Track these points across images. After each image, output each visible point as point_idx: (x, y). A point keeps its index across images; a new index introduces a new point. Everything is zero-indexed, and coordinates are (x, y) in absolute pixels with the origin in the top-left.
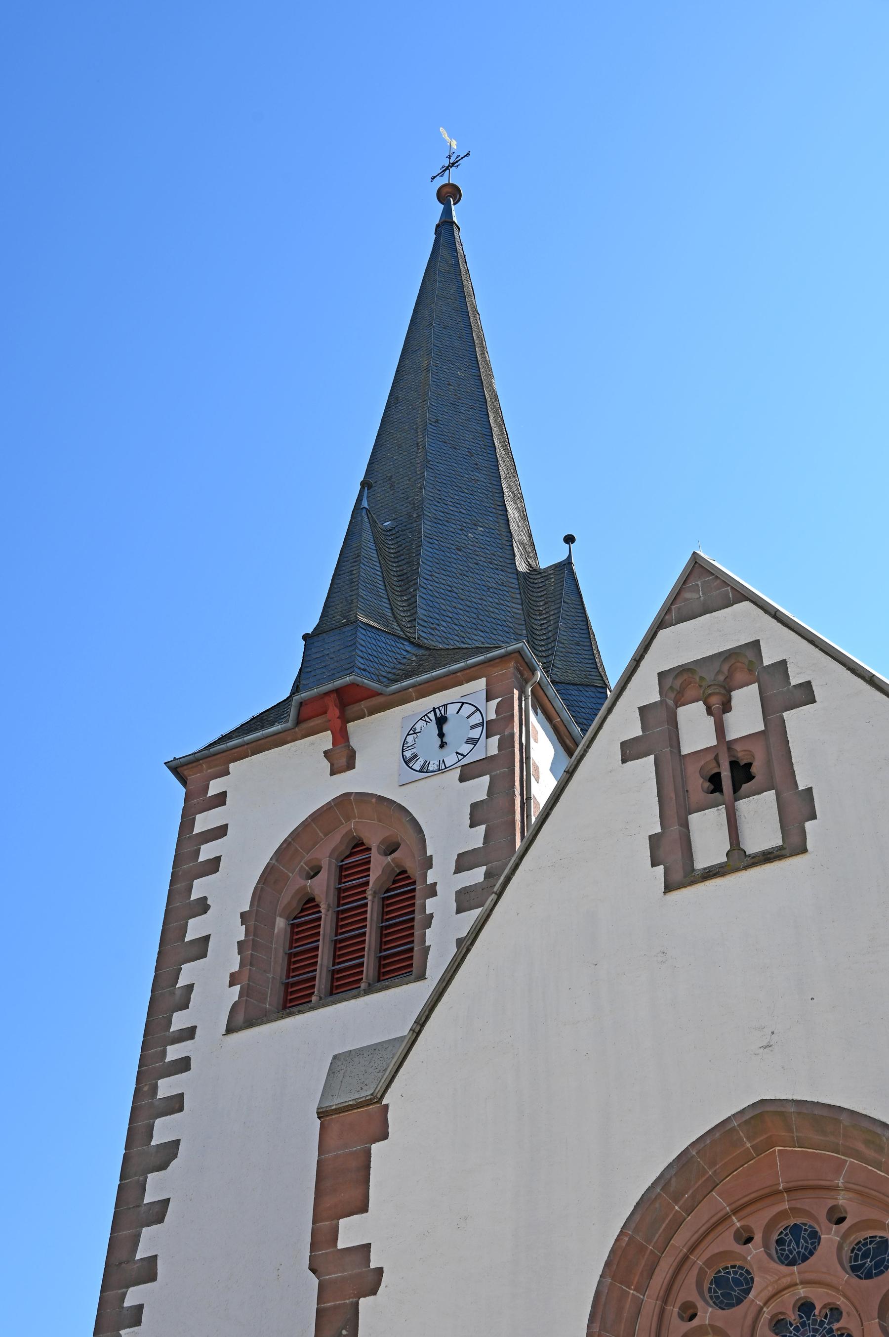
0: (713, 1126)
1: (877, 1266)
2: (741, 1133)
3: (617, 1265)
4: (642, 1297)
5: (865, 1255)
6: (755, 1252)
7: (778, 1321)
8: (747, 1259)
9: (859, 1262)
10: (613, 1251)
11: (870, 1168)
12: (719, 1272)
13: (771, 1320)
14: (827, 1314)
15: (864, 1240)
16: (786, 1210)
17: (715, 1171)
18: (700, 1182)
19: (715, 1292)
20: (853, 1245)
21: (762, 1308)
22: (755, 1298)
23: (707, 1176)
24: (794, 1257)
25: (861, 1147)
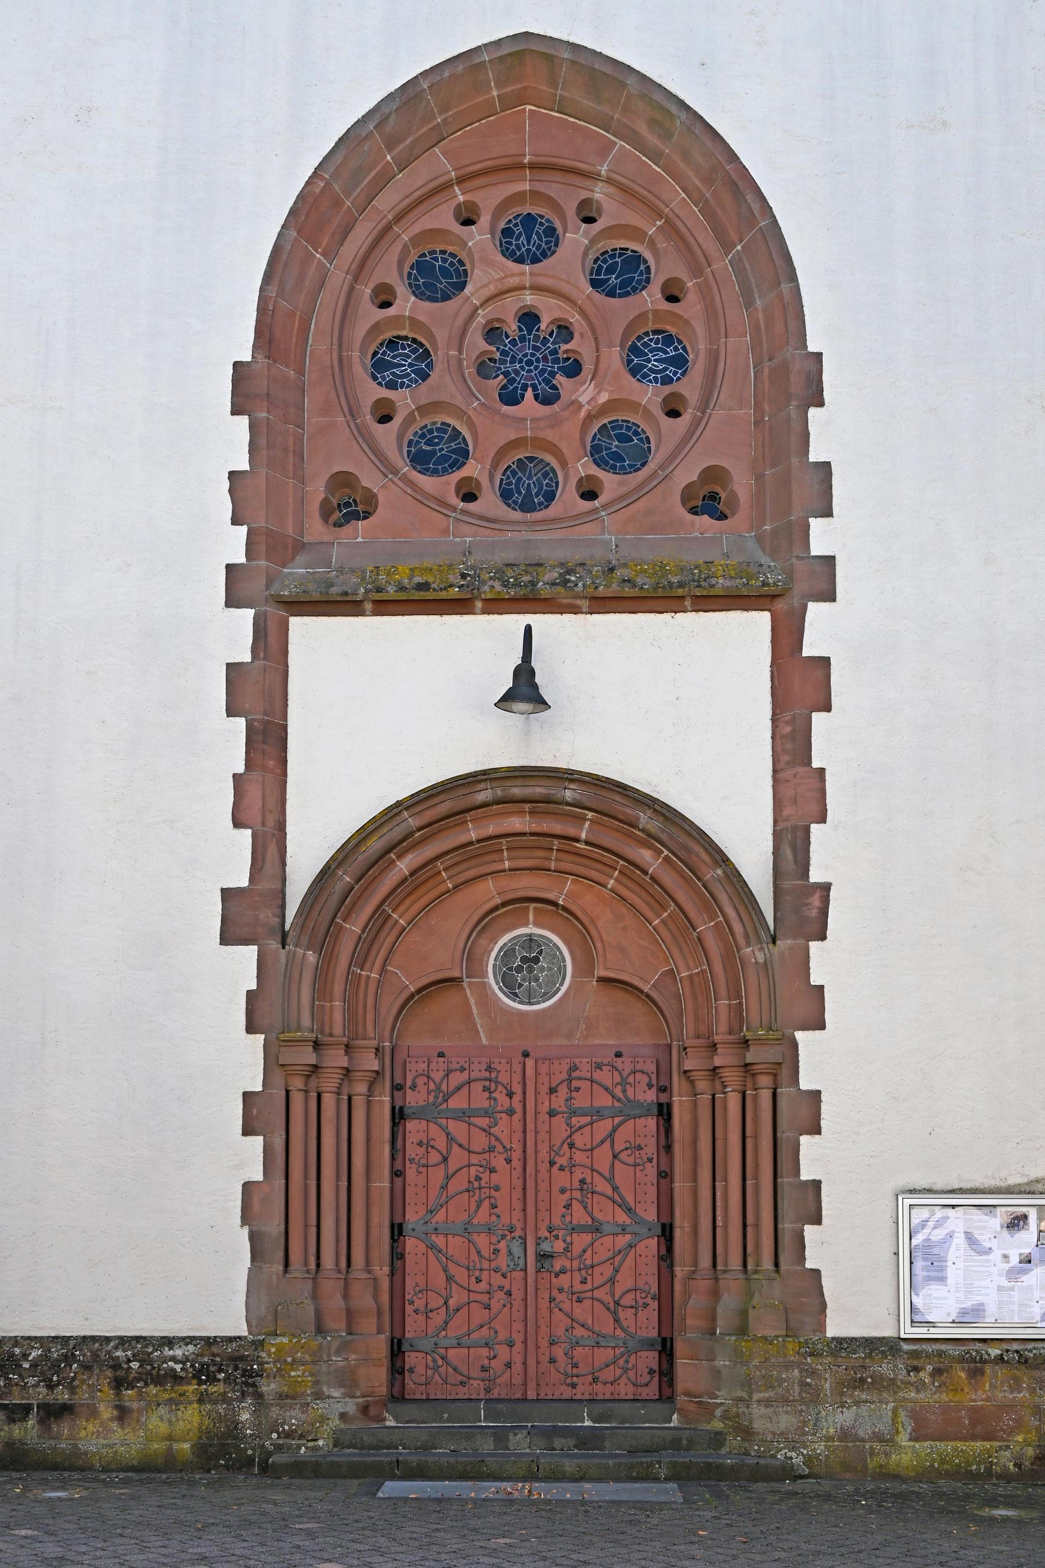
0: (455, 54)
1: (624, 284)
2: (490, 73)
3: (307, 215)
4: (328, 265)
5: (610, 270)
6: (478, 237)
7: (492, 330)
8: (467, 244)
9: (602, 277)
10: (301, 196)
11: (644, 158)
12: (424, 255)
13: (485, 326)
14: (553, 331)
15: (612, 250)
16: (525, 192)
17: (446, 119)
18: (424, 130)
19: (416, 279)
20: (598, 254)
21: (477, 309)
22: (472, 294)
23: (434, 123)
24: (522, 255)
25: (642, 128)
